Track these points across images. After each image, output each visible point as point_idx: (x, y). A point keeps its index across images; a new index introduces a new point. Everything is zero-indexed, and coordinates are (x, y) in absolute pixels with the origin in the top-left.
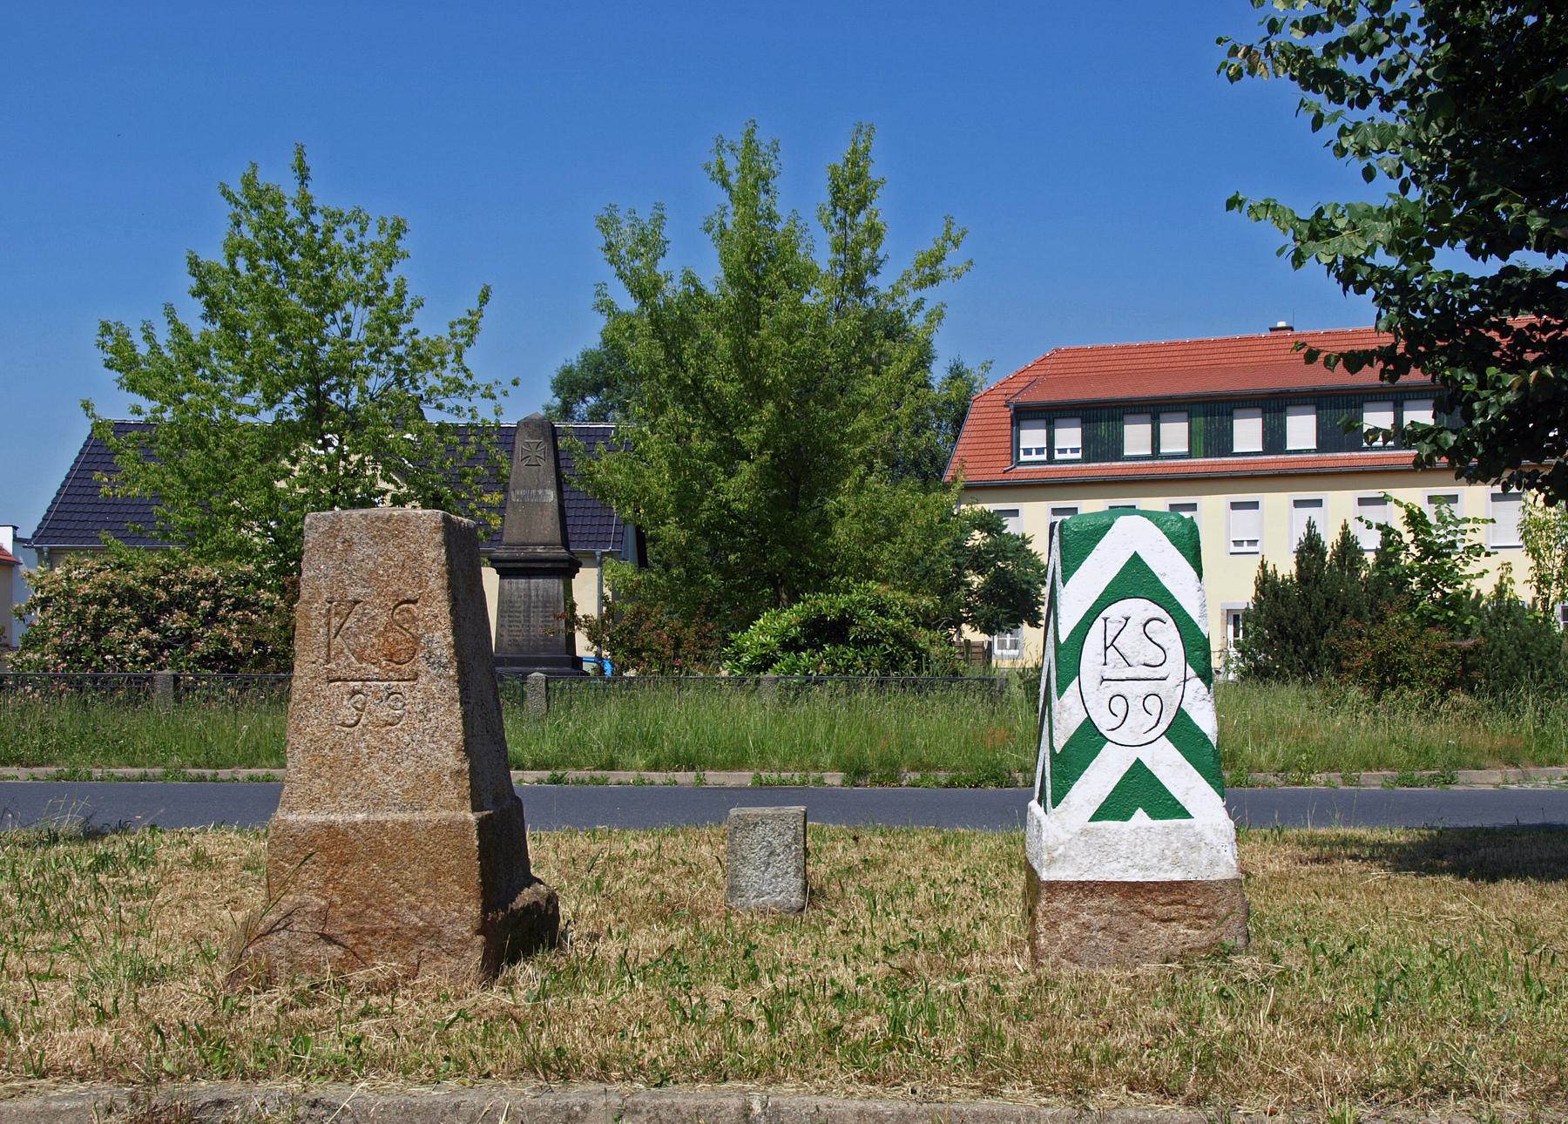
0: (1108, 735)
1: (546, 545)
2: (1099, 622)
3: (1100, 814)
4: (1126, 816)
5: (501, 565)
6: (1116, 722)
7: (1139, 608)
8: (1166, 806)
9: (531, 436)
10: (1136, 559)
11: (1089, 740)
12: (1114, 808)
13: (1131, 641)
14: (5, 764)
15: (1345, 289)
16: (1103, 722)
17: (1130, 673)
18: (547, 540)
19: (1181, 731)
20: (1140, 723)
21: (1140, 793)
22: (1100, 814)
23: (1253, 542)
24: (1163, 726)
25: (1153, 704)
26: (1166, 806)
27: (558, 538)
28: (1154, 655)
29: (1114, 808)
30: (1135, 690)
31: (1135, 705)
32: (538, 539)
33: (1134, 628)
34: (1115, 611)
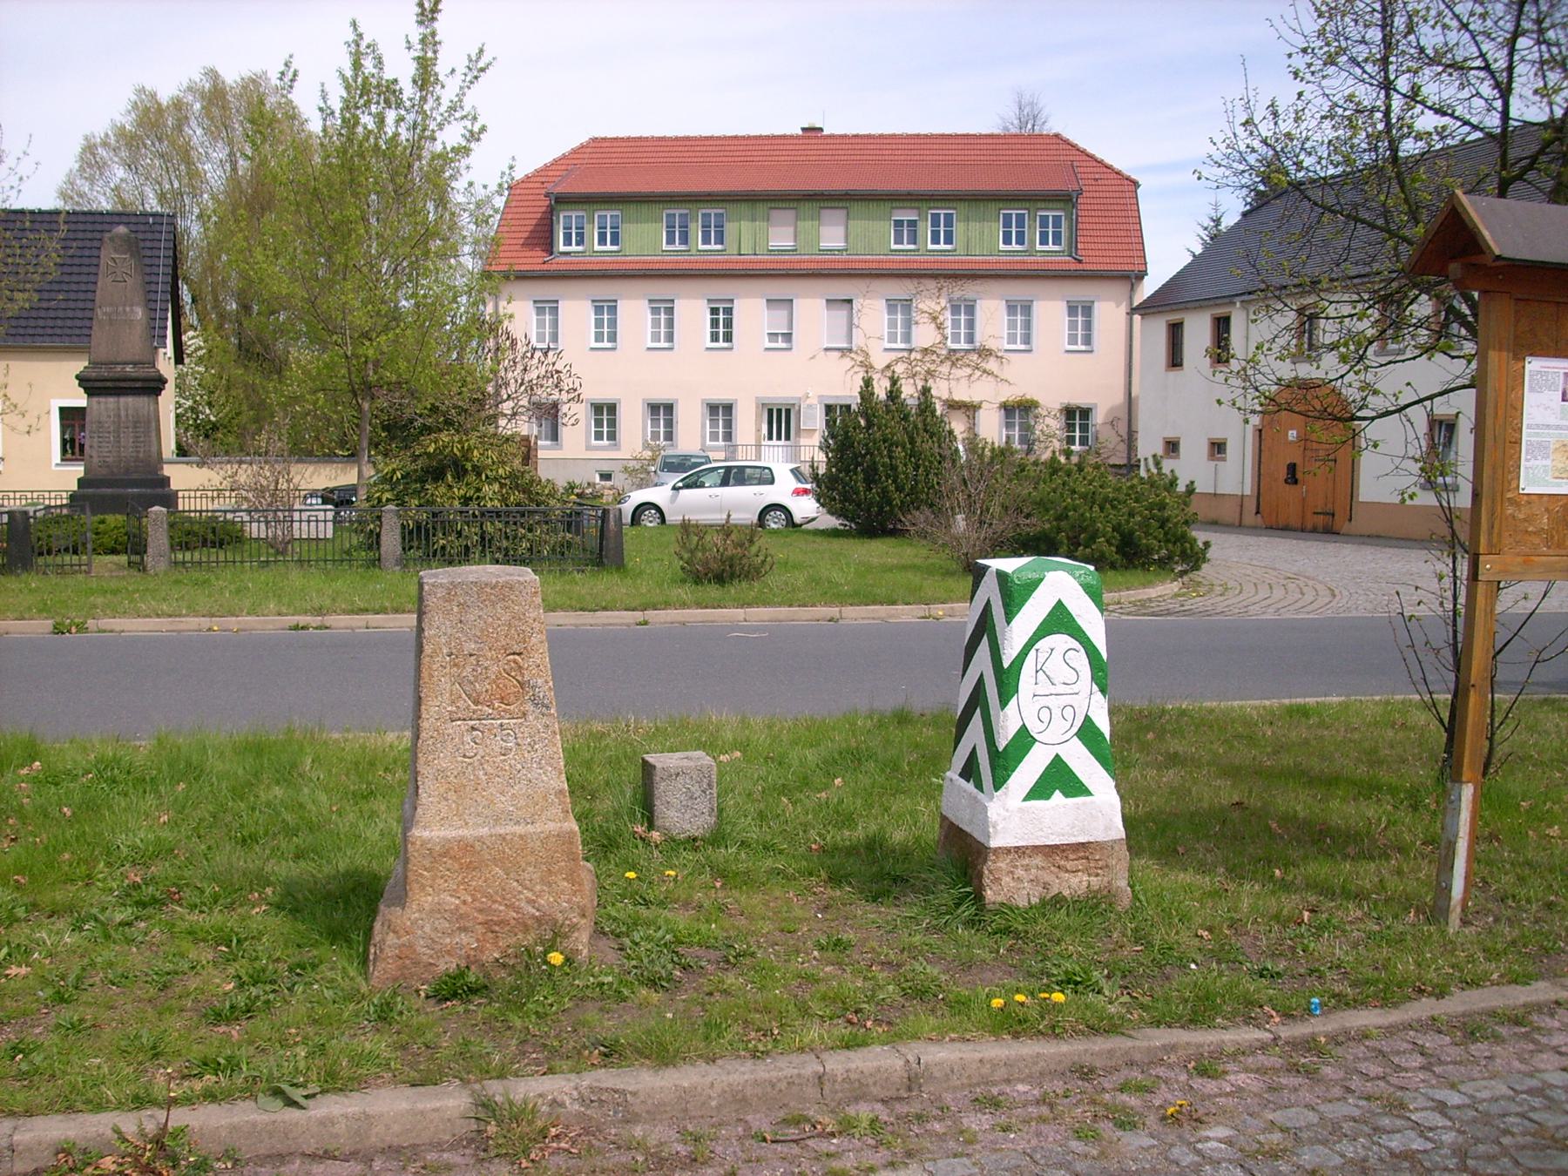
1: (135, 364)
2: (1033, 652)
5: (89, 384)
7: (1060, 641)
8: (1074, 787)
9: (116, 251)
10: (1060, 601)
11: (1024, 740)
12: (1040, 791)
13: (1055, 666)
16: (1034, 728)
17: (1053, 690)
19: (1087, 732)
21: (1059, 779)
24: (1075, 729)
25: (1068, 712)
26: (1074, 787)
29: (1040, 791)
30: (1054, 703)
31: (1056, 713)
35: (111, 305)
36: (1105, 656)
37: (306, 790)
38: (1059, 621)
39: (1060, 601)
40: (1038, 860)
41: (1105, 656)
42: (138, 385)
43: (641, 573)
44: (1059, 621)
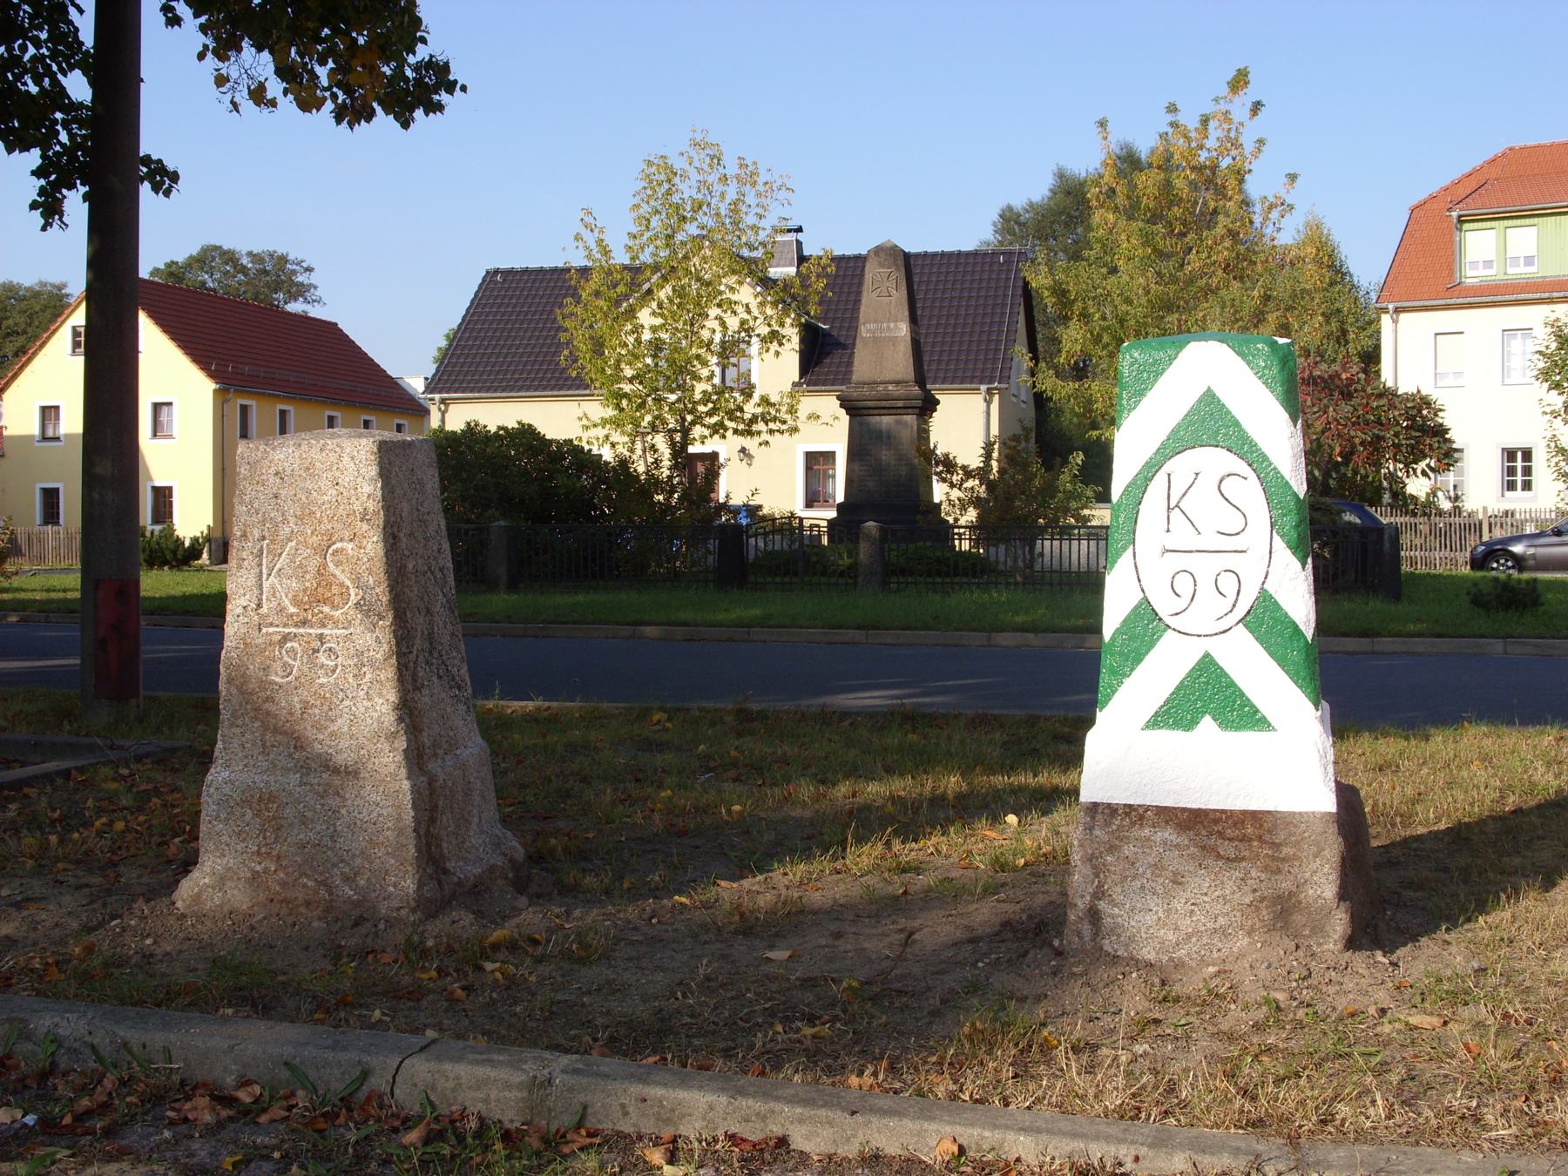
0: (1168, 620)
1: (897, 383)
2: (1161, 477)
3: (1159, 720)
4: (1190, 725)
6: (1181, 604)
7: (1213, 461)
8: (1239, 712)
10: (1209, 389)
12: (1177, 712)
13: (1202, 503)
14: (8, 764)
15: (439, 108)
16: (1164, 605)
18: (899, 377)
19: (1264, 619)
20: (1208, 612)
21: (1208, 697)
22: (1159, 720)
23: (1458, 374)
26: (1239, 712)
27: (909, 374)
28: (1234, 522)
29: (1177, 712)
30: (1206, 567)
31: (1205, 586)
32: (888, 376)
33: (1207, 484)
34: (1181, 466)
35: (875, 321)
36: (1358, 521)
37: (323, 680)
38: (1209, 423)
39: (1209, 389)
40: (1168, 834)
41: (1358, 521)
42: (900, 404)
43: (592, 338)
44: (1209, 423)
